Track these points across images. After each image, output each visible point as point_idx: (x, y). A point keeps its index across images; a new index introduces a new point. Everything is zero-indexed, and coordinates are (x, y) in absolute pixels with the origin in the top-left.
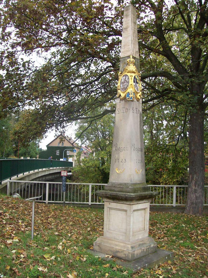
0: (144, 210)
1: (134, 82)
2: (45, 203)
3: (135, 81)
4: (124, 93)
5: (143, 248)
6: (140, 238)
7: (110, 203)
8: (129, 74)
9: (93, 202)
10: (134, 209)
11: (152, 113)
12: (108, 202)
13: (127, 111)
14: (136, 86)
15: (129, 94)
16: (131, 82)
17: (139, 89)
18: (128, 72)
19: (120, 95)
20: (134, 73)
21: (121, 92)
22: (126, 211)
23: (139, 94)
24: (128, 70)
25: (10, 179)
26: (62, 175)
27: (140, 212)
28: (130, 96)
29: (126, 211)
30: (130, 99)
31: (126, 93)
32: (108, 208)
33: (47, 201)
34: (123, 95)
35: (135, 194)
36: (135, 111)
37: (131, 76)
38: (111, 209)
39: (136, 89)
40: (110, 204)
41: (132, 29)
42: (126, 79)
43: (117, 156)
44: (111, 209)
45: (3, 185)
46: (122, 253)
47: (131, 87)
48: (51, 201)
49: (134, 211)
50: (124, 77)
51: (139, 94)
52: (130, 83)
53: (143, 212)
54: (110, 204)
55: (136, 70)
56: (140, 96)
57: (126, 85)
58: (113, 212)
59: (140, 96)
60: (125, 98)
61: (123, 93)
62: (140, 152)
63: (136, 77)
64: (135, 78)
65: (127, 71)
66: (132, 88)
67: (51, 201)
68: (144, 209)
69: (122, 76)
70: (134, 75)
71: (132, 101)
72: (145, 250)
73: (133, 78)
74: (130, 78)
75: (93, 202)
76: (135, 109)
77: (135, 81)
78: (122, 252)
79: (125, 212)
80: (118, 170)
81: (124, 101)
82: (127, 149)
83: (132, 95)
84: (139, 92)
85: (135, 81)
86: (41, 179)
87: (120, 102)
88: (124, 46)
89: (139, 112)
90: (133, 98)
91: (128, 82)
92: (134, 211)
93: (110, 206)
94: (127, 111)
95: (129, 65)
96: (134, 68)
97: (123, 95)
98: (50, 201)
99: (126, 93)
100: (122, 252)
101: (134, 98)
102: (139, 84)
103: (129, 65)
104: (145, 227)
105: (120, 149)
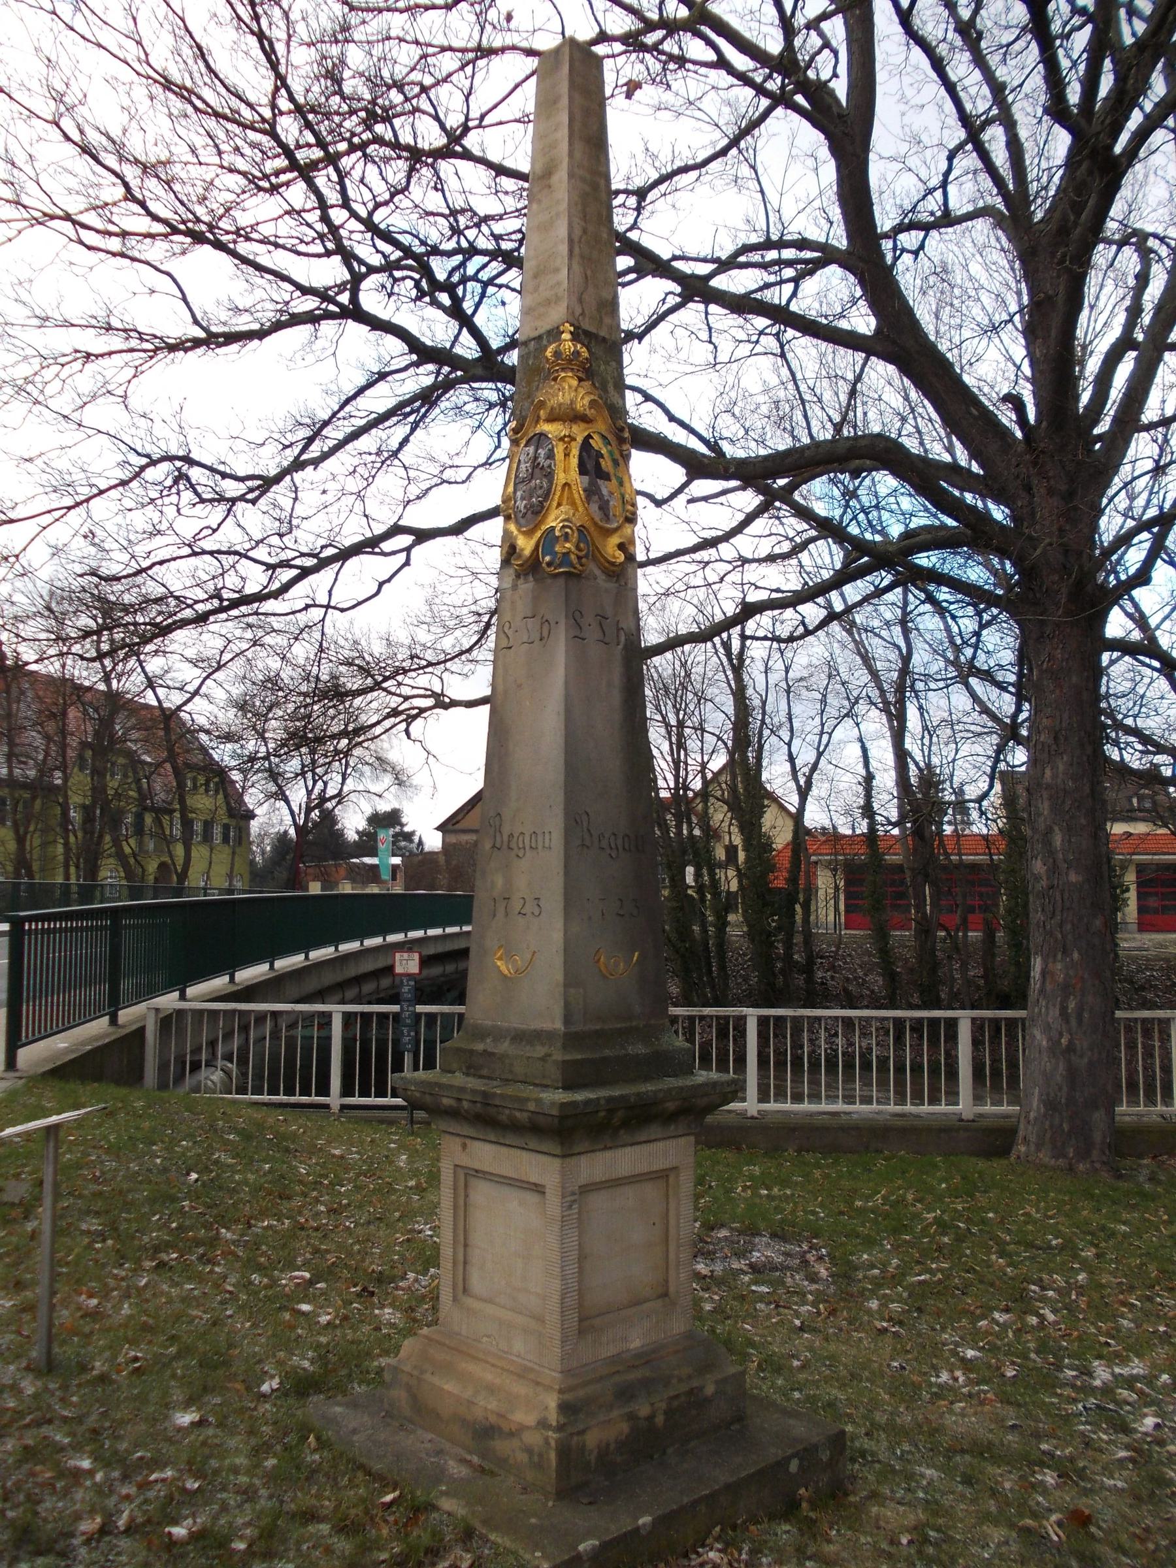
1: (583, 470)
3: (590, 465)
4: (529, 533)
5: (644, 1411)
6: (636, 1344)
7: (468, 1141)
8: (552, 429)
10: (582, 1182)
12: (458, 1140)
13: (545, 634)
17: (618, 511)
18: (550, 420)
20: (583, 419)
25: (183, 997)
26: (399, 970)
27: (629, 1196)
28: (557, 548)
30: (560, 566)
31: (538, 534)
33: (334, 1099)
36: (592, 633)
37: (562, 439)
39: (594, 507)
40: (464, 1146)
43: (500, 881)
45: (123, 1027)
46: (515, 1443)
50: (531, 449)
52: (560, 478)
53: (651, 1191)
54: (464, 1146)
55: (593, 403)
61: (524, 533)
63: (597, 443)
64: (586, 445)
68: (663, 1176)
69: (523, 442)
70: (579, 432)
72: (660, 1419)
74: (559, 451)
78: (512, 1434)
79: (532, 1198)
80: (508, 956)
81: (531, 578)
84: (615, 525)
85: (590, 465)
86: (351, 993)
89: (623, 639)
90: (573, 557)
91: (549, 475)
93: (465, 1160)
94: (545, 634)
96: (582, 392)
99: (538, 534)
100: (512, 1434)
101: (579, 558)
102: (614, 481)
103: (555, 379)
104: (667, 1281)
105: (513, 845)
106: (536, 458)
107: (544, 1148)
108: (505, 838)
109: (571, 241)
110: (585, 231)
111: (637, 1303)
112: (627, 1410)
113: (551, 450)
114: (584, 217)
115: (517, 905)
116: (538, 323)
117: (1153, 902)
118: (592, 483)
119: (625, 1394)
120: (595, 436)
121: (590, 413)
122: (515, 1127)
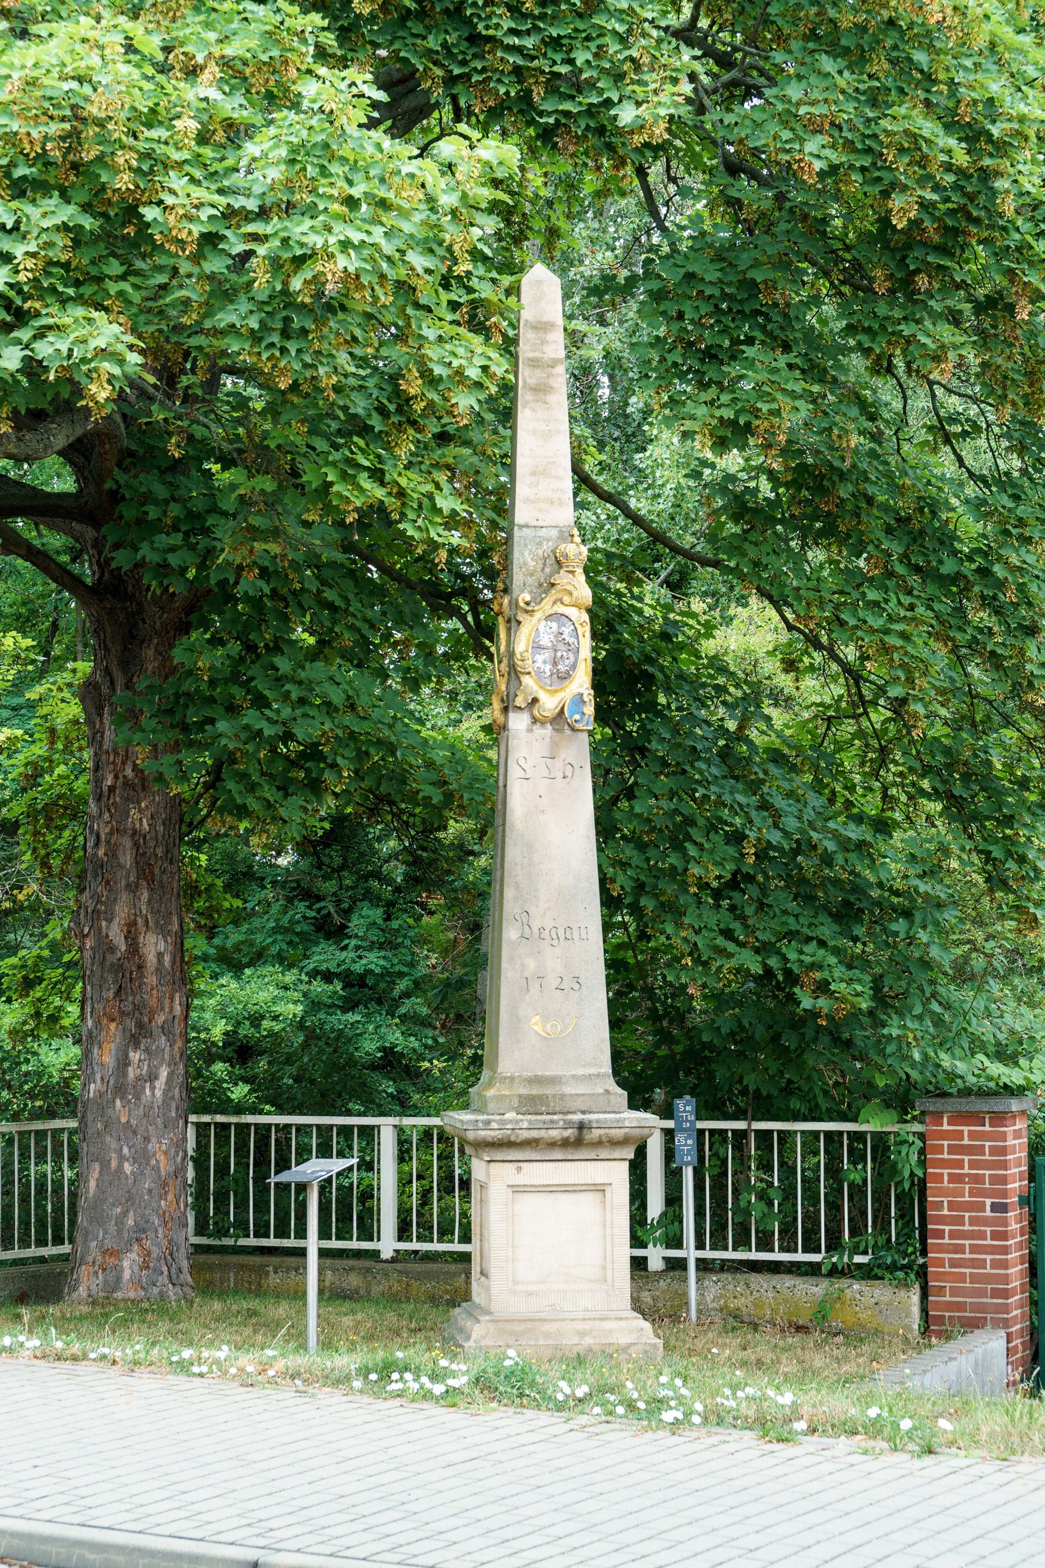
19: (535, 700)
21: (535, 687)
24: (575, 593)
38: (517, 1190)
43: (531, 964)
44: (517, 1190)
82: (584, 936)
87: (530, 730)
93: (520, 1179)
97: (549, 704)
108: (535, 930)
116: (540, 516)
122: (599, 1143)
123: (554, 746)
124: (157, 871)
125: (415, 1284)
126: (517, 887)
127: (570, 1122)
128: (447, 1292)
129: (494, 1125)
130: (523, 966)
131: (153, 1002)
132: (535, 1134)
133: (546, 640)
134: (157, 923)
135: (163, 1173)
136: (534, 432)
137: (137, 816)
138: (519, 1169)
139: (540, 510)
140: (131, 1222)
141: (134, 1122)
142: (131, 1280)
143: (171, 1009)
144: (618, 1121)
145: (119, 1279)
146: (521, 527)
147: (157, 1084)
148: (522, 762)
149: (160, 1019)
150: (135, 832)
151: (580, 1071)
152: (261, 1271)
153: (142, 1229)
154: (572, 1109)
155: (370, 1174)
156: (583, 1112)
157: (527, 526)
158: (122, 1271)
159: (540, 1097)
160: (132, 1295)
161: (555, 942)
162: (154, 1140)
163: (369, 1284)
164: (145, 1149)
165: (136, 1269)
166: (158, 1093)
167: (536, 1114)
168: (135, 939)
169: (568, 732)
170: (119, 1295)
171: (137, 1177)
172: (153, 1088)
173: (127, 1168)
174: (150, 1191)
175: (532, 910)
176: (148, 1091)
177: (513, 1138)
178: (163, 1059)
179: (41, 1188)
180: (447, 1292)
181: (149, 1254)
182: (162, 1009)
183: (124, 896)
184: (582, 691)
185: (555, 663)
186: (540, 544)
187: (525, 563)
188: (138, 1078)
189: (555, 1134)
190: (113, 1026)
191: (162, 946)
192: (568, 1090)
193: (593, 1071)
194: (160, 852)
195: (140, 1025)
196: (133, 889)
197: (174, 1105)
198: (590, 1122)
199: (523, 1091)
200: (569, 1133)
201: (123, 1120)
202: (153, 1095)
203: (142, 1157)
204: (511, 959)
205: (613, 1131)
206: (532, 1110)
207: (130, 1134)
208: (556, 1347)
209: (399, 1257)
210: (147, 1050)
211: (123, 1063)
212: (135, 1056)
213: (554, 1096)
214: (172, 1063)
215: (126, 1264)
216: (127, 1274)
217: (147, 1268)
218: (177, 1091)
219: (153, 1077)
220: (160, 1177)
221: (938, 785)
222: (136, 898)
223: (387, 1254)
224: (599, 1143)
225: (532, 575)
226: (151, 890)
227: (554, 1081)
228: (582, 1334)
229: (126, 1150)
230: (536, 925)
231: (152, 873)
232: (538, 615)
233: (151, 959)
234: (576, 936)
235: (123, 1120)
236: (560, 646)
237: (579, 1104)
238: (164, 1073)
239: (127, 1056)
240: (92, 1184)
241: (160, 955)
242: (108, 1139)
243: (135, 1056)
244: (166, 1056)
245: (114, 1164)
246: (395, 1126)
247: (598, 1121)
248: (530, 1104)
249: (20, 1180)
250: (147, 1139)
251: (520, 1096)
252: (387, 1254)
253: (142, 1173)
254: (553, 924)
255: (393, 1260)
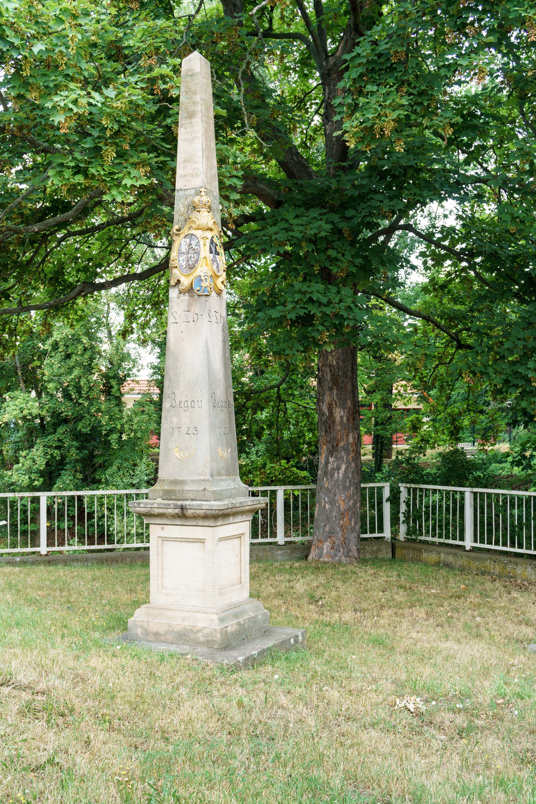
0: (239, 539)
1: (211, 252)
2: (462, 548)
3: (213, 250)
8: (198, 233)
9: (257, 538)
11: (324, 689)
14: (214, 260)
15: (199, 279)
16: (205, 251)
19: (179, 281)
21: (179, 274)
22: (201, 541)
23: (221, 280)
24: (198, 223)
29: (201, 541)
30: (203, 292)
31: (192, 277)
32: (160, 540)
34: (185, 282)
35: (220, 503)
36: (213, 319)
38: (165, 539)
39: (215, 267)
41: (202, 121)
42: (193, 246)
43: (175, 421)
44: (165, 539)
47: (204, 264)
48: (260, 540)
49: (221, 539)
51: (221, 280)
52: (202, 255)
53: (236, 542)
54: (163, 528)
56: (223, 282)
57: (193, 260)
58: (170, 547)
59: (223, 282)
60: (190, 290)
62: (225, 410)
63: (215, 240)
64: (212, 242)
65: (194, 226)
66: (207, 265)
67: (260, 540)
68: (240, 536)
70: (209, 234)
71: (208, 295)
73: (208, 242)
74: (202, 242)
75: (257, 537)
76: (213, 313)
77: (214, 251)
79: (198, 545)
82: (200, 406)
83: (207, 284)
85: (213, 250)
87: (178, 297)
88: (185, 162)
90: (209, 289)
91: (198, 253)
92: (221, 539)
93: (163, 534)
95: (199, 211)
96: (210, 218)
97: (185, 282)
98: (255, 541)
99: (192, 277)
103: (199, 211)
106: (190, 244)
107: (206, 524)
108: (178, 403)
109: (203, 150)
110: (206, 144)
111: (233, 585)
112: (237, 621)
113: (198, 242)
114: (206, 140)
115: (184, 430)
116: (187, 184)
117: (467, 484)
118: (214, 257)
119: (236, 616)
120: (215, 237)
121: (213, 227)
122: (195, 517)
123: (190, 304)
124: (339, 381)
125: (472, 562)
126: (170, 380)
127: (177, 505)
128: (483, 567)
129: (142, 505)
130: (171, 421)
131: (338, 437)
132: (161, 511)
133: (184, 249)
134: (340, 403)
135: (342, 509)
136: (185, 140)
137: (331, 359)
138: (163, 528)
139: (187, 181)
140: (327, 529)
141: (330, 487)
142: (326, 554)
143: (347, 440)
144: (199, 506)
145: (322, 552)
146: (178, 190)
147: (340, 471)
148: (174, 314)
149: (342, 444)
150: (330, 366)
151: (196, 478)
152: (420, 551)
153: (331, 533)
154: (187, 498)
155: (32, 529)
156: (192, 500)
157: (181, 190)
158: (323, 549)
159: (172, 491)
160: (326, 560)
161: (186, 409)
162: (338, 495)
163: (456, 560)
164: (334, 499)
165: (329, 549)
166: (341, 475)
167: (170, 500)
168: (332, 410)
169: (196, 297)
170: (321, 559)
171: (331, 510)
172: (338, 473)
173: (327, 506)
174: (336, 516)
175: (176, 392)
176: (336, 475)
177: (152, 513)
178: (343, 461)
179: (434, 508)
180: (483, 567)
181: (334, 543)
182: (343, 440)
183: (328, 393)
184: (201, 274)
185: (188, 261)
186: (186, 198)
187: (179, 210)
188: (333, 469)
189: (170, 511)
190: (324, 447)
191: (342, 414)
192: (187, 488)
193: (202, 478)
194: (340, 373)
195: (333, 446)
196: (331, 389)
197: (348, 480)
198: (186, 505)
199: (166, 487)
200: (177, 511)
201: (326, 486)
202: (338, 476)
203: (333, 502)
204: (166, 418)
205: (198, 511)
206: (169, 498)
207: (328, 492)
208: (169, 625)
209: (474, 549)
210: (336, 457)
211: (327, 463)
212: (331, 460)
213: (179, 490)
214: (348, 463)
215: (325, 546)
216: (325, 551)
217: (333, 549)
218: (350, 475)
219: (339, 468)
220: (340, 510)
221: (380, 313)
222: (332, 393)
223: (468, 548)
224: (195, 517)
225: (182, 215)
226: (337, 389)
227: (182, 482)
228: (184, 619)
229: (327, 499)
230: (178, 400)
231: (338, 382)
232: (182, 236)
233: (338, 419)
234: (196, 405)
235: (326, 486)
236: (191, 251)
237: (190, 496)
238: (343, 467)
239: (328, 459)
240: (316, 512)
241: (342, 417)
242: (321, 494)
243: (331, 460)
244: (345, 460)
245: (323, 504)
246: (472, 492)
247: (189, 505)
248: (168, 495)
249: (68, 514)
250: (335, 495)
251: (163, 490)
252: (468, 548)
253: (333, 509)
254: (185, 399)
255: (470, 551)
